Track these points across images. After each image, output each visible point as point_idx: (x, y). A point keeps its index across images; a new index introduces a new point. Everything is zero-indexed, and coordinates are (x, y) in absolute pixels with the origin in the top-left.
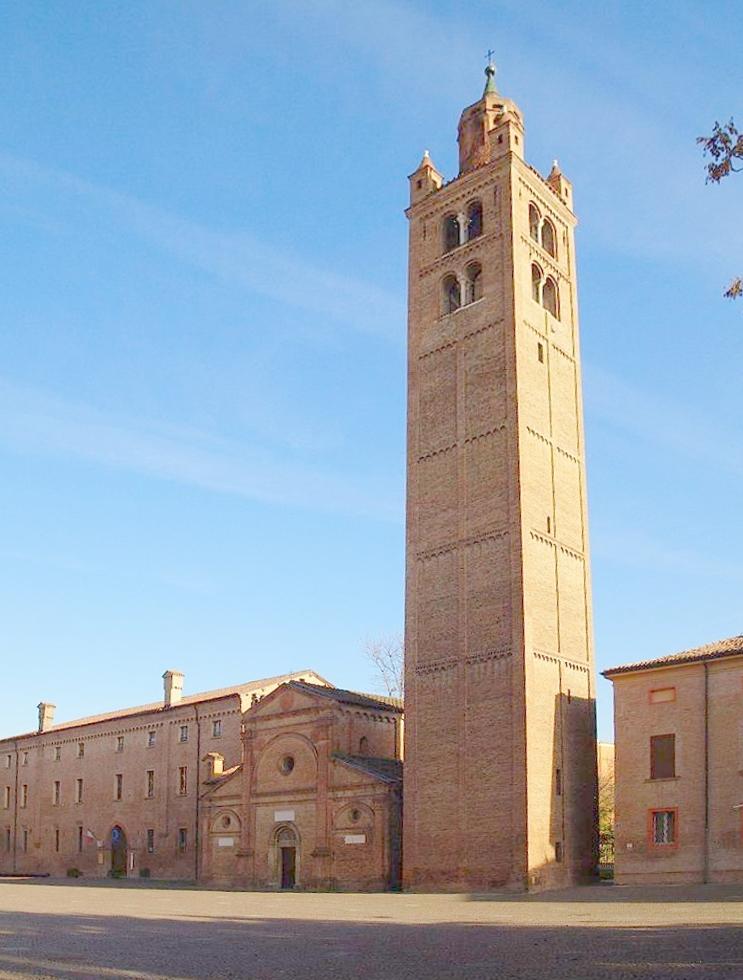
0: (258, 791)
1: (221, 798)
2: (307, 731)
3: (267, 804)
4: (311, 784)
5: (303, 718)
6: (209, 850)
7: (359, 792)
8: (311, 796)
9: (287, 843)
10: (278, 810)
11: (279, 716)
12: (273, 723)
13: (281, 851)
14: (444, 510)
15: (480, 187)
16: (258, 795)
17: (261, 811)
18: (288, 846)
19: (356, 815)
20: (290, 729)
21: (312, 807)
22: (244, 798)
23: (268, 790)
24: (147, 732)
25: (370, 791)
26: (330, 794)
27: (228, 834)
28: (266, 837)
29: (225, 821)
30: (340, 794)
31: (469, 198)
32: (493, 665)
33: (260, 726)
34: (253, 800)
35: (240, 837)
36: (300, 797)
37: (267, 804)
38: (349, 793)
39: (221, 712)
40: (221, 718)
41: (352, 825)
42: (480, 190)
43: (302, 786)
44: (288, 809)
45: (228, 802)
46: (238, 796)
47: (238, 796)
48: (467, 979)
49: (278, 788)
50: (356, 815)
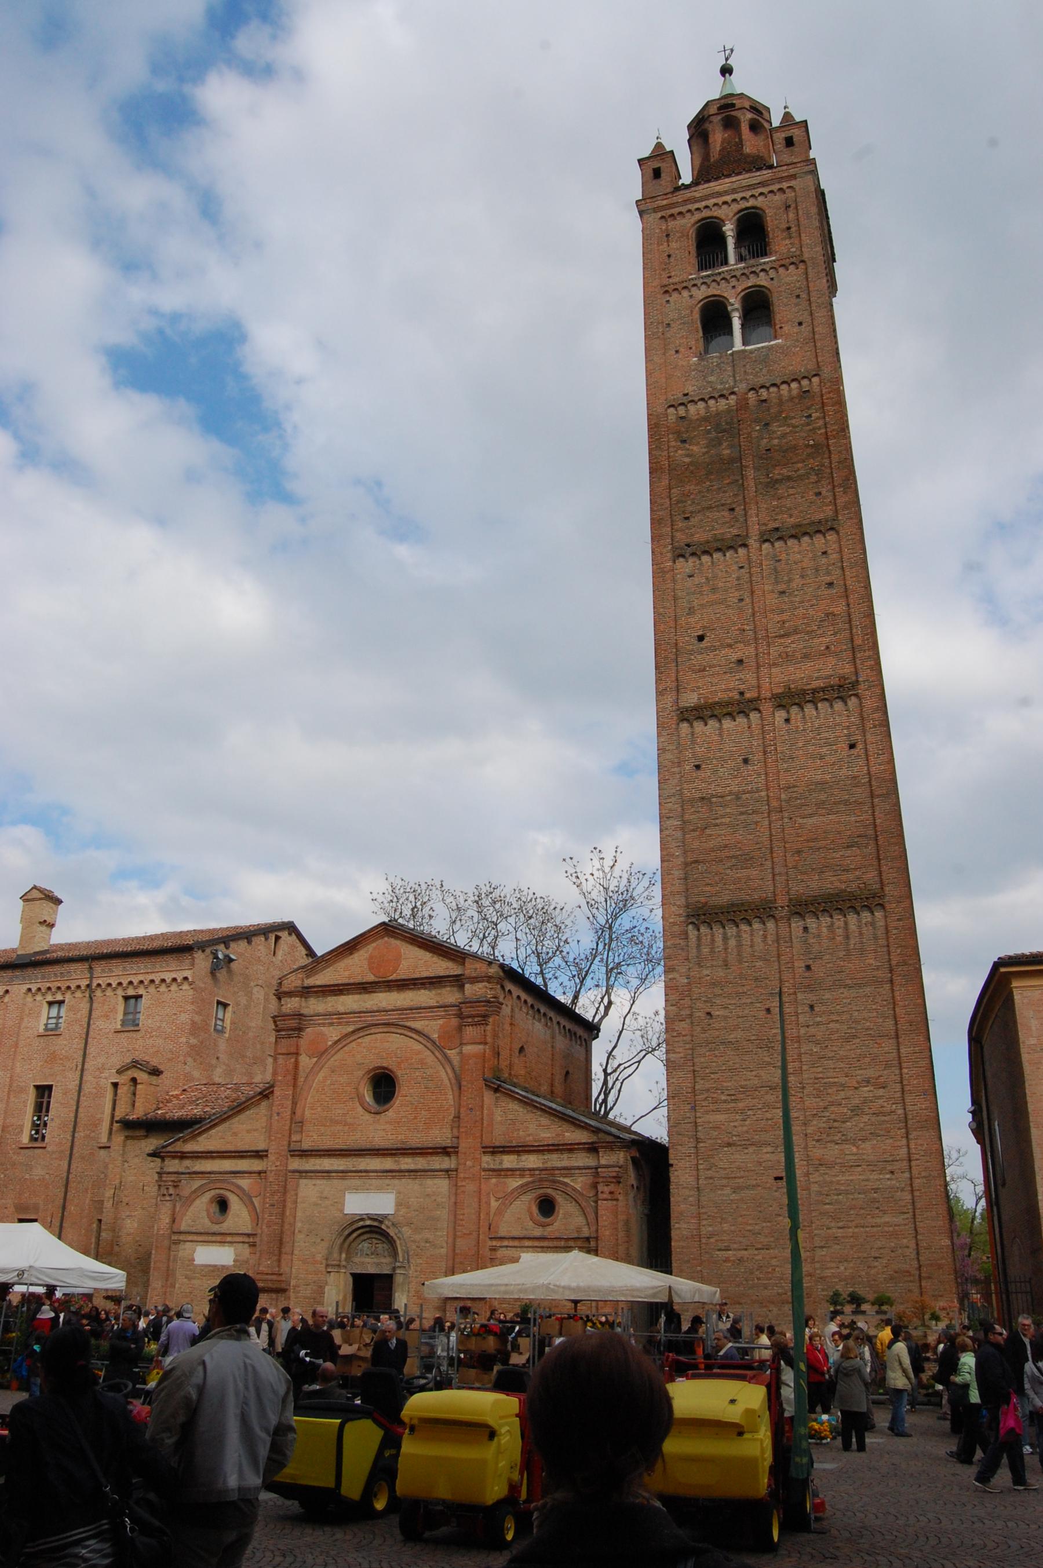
0: (305, 1146)
1: (209, 1155)
2: (433, 1027)
3: (327, 1174)
4: (441, 1136)
5: (424, 997)
6: (169, 1275)
7: (556, 1160)
8: (446, 1163)
9: (370, 1264)
10: (356, 1189)
11: (364, 988)
12: (349, 1002)
13: (350, 1279)
14: (730, 646)
15: (761, 194)
16: (304, 1154)
17: (309, 1190)
18: (372, 1270)
19: (547, 1206)
20: (392, 1018)
21: (442, 1185)
22: (271, 1157)
23: (328, 1143)
24: (120, 992)
25: (582, 1160)
26: (487, 1160)
27: (220, 1238)
28: (320, 1251)
29: (215, 1208)
30: (509, 1161)
31: (743, 206)
32: (738, 936)
33: (315, 1006)
34: (295, 1164)
35: (253, 1245)
36: (407, 1163)
37: (327, 1174)
38: (532, 1161)
39: (64, 986)
40: (141, 991)
41: (538, 1232)
42: (760, 199)
43: (416, 1139)
44: (379, 1189)
45: (227, 1165)
46: (259, 1155)
47: (259, 1155)
48: (2, 1164)
49: (356, 1141)
50: (547, 1206)
